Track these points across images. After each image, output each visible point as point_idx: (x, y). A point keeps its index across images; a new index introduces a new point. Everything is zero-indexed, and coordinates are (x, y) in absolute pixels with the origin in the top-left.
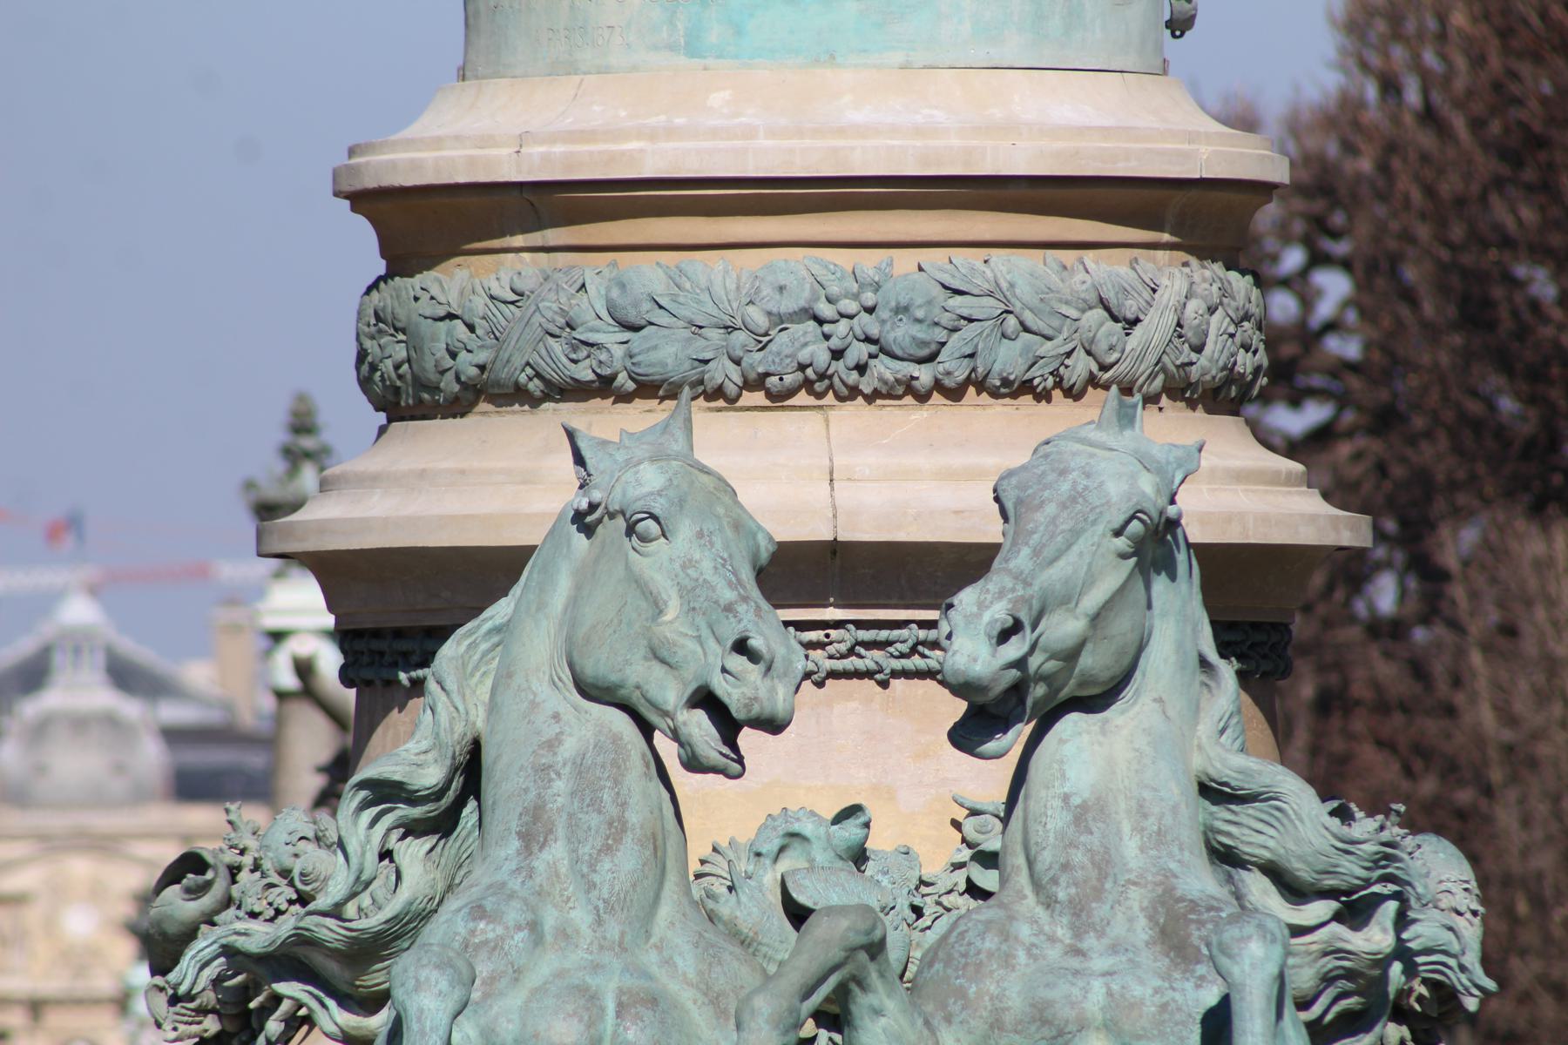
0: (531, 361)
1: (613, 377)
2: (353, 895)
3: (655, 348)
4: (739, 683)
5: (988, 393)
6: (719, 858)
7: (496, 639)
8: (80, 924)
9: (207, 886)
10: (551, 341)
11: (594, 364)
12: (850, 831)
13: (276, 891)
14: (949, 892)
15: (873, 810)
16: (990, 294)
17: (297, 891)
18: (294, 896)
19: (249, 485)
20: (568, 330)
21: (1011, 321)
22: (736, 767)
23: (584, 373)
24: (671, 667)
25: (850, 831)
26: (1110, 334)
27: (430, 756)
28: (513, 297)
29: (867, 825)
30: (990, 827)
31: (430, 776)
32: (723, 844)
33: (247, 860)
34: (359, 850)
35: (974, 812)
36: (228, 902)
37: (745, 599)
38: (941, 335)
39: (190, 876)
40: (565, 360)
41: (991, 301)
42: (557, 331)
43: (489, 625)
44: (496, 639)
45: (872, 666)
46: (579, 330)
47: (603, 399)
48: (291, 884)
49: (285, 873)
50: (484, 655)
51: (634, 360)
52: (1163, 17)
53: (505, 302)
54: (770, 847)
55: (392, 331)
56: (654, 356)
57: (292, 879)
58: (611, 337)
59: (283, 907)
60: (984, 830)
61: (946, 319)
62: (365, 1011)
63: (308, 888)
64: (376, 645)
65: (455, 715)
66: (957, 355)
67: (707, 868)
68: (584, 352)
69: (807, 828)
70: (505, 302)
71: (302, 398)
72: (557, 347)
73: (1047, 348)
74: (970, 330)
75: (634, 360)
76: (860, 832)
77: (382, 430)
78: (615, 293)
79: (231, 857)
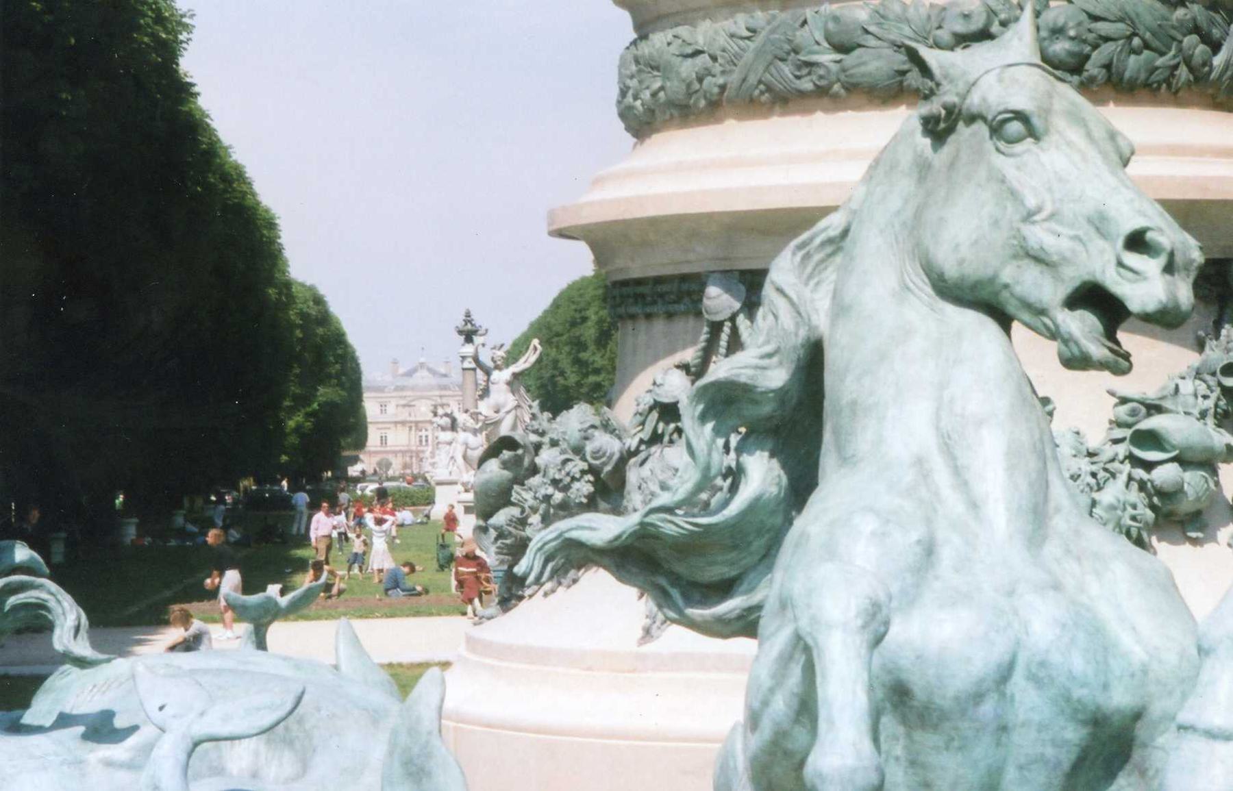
0: (763, 79)
1: (830, 86)
3: (864, 63)
4: (1138, 277)
7: (829, 249)
8: (423, 409)
10: (780, 63)
11: (814, 78)
14: (1113, 460)
16: (1121, 20)
17: (590, 465)
18: (586, 467)
19: (457, 327)
20: (793, 54)
21: (1136, 41)
22: (1125, 364)
23: (807, 85)
24: (1047, 264)
26: (1203, 52)
27: (775, 359)
28: (748, 34)
31: (777, 377)
33: (546, 440)
34: (705, 448)
38: (1088, 49)
39: (505, 452)
40: (791, 76)
41: (1121, 26)
42: (784, 56)
43: (822, 237)
44: (829, 249)
46: (803, 53)
47: (594, 261)
50: (817, 265)
51: (848, 73)
53: (743, 38)
55: (650, 69)
56: (863, 69)
57: (584, 455)
58: (827, 58)
59: (578, 476)
61: (1091, 37)
62: (274, 265)
63: (597, 462)
64: (640, 290)
65: (799, 319)
66: (1099, 64)
68: (805, 71)
70: (743, 38)
71: (468, 310)
72: (787, 69)
73: (1160, 61)
74: (1107, 49)
75: (848, 73)
77: (635, 145)
78: (831, 26)
79: (534, 438)
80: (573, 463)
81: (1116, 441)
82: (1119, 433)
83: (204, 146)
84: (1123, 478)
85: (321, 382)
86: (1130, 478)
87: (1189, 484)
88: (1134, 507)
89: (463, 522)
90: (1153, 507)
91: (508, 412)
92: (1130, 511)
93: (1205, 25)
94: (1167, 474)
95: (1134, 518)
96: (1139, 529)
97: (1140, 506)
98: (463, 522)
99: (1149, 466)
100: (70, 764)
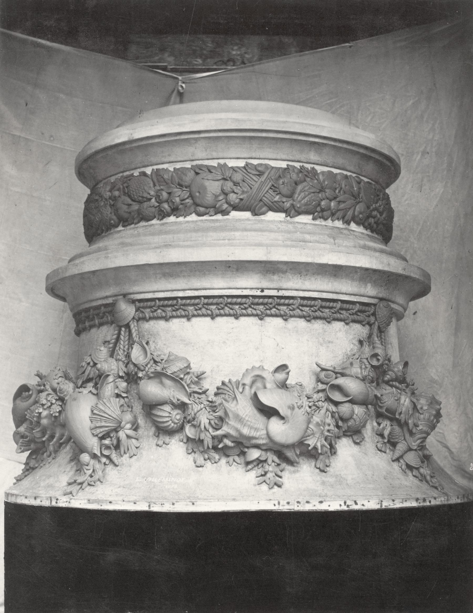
2: (309, 422)
5: (388, 185)
6: (225, 388)
9: (30, 396)
12: (280, 376)
13: (50, 396)
15: (292, 367)
18: (58, 398)
25: (280, 376)
29: (288, 373)
30: (331, 376)
32: (227, 381)
35: (323, 370)
36: (36, 402)
37: (120, 348)
45: (282, 313)
48: (56, 394)
49: (54, 390)
52: (248, 220)
54: (248, 381)
60: (329, 377)
63: (62, 395)
67: (220, 391)
69: (265, 375)
76: (286, 376)
80: (52, 396)
81: (318, 392)
82: (321, 386)
83: (103, 256)
84: (323, 411)
85: (125, 328)
86: (327, 410)
87: (357, 415)
88: (329, 425)
89: (196, 470)
90: (338, 426)
91: (302, 310)
92: (327, 428)
93: (68, 447)
94: (345, 409)
95: (329, 431)
96: (331, 436)
97: (332, 425)
98: (196, 470)
99: (336, 404)
100: (281, 76)
